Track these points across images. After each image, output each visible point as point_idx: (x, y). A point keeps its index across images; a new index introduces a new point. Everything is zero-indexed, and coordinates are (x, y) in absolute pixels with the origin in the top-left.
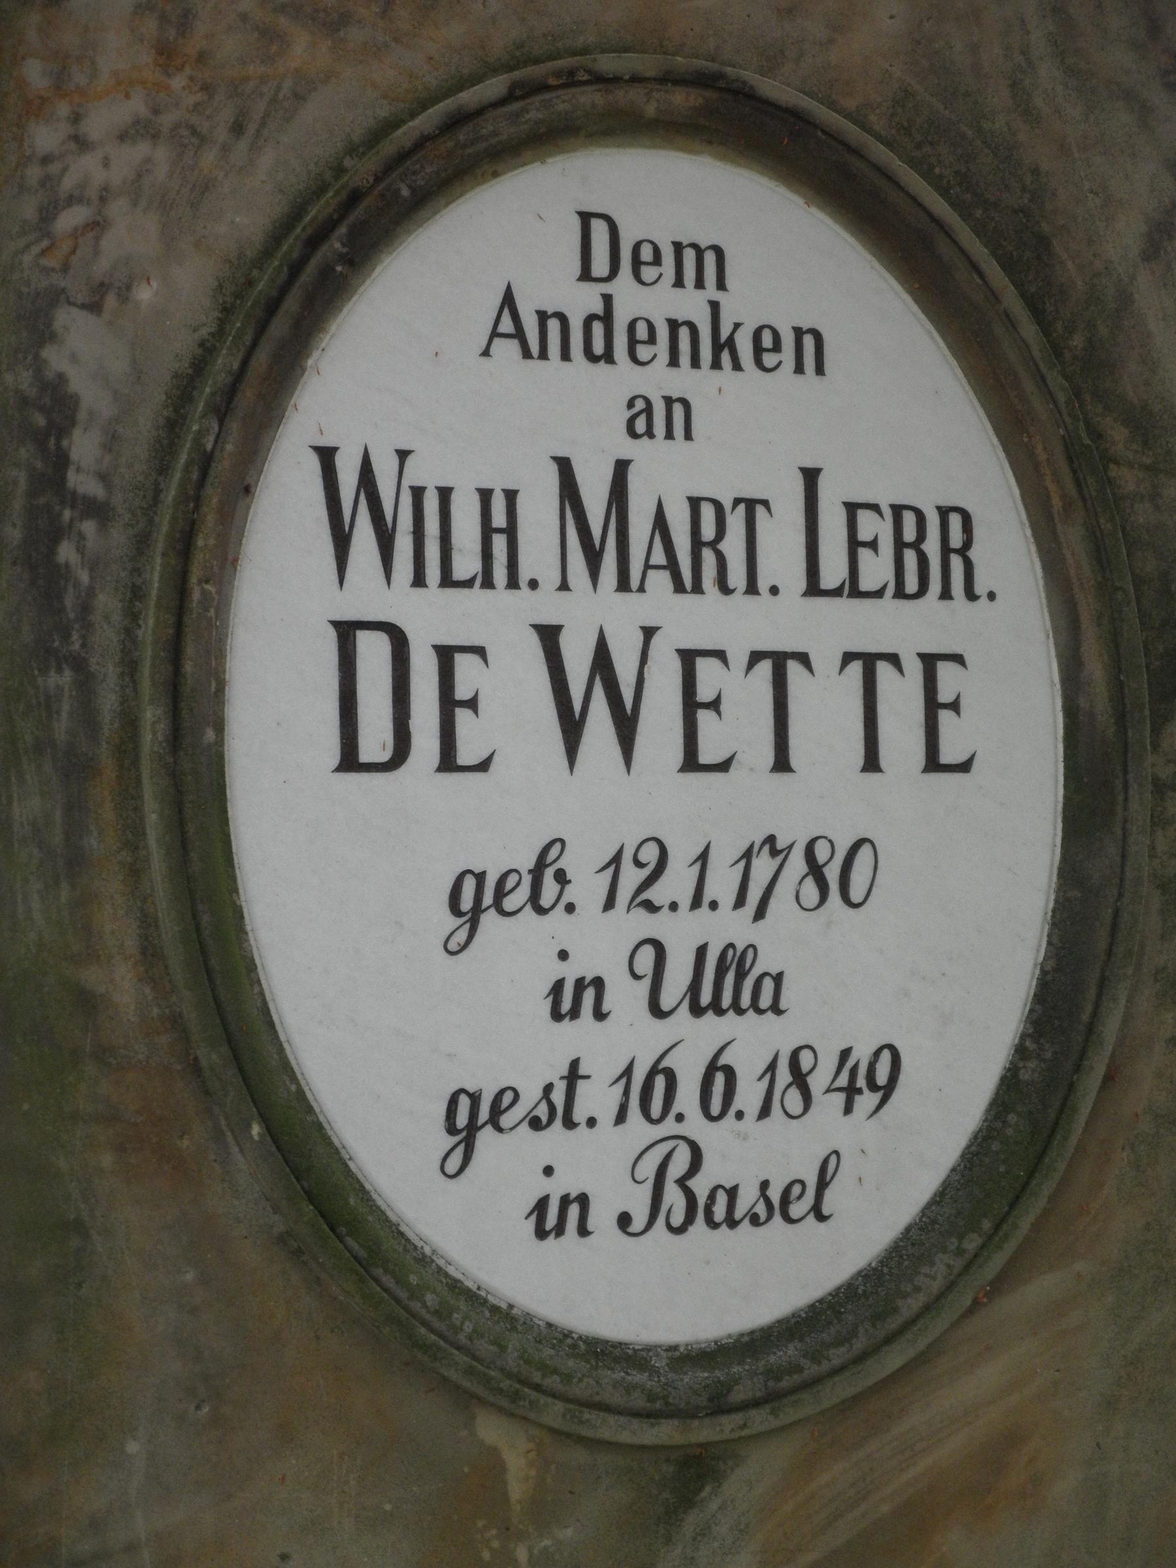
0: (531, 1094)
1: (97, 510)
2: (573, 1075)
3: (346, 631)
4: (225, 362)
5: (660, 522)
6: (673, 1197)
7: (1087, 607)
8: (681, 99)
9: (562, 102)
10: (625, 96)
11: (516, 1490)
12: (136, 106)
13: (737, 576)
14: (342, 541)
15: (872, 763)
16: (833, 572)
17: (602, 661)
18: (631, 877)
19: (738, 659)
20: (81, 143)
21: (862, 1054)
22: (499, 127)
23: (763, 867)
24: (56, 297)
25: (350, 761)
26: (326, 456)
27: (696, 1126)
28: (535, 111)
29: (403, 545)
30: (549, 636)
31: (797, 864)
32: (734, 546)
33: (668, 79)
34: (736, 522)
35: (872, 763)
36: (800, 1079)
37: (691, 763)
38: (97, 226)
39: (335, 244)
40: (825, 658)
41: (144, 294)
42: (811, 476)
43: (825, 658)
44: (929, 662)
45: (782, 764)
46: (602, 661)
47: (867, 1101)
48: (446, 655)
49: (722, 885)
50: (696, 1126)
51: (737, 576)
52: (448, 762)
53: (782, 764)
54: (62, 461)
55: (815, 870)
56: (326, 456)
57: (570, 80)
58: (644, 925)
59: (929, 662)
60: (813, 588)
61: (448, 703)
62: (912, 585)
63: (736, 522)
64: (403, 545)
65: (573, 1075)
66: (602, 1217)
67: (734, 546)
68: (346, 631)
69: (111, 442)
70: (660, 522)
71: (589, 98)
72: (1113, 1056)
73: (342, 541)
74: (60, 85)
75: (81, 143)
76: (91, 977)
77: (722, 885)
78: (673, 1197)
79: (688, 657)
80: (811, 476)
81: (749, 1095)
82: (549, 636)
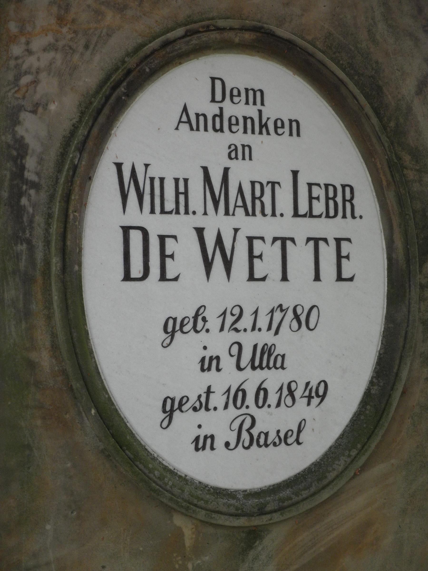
0: (193, 399)
1: (35, 186)
2: (209, 391)
3: (126, 230)
4: (82, 132)
5: (240, 190)
6: (245, 436)
7: (396, 221)
8: (248, 36)
9: (205, 37)
10: (227, 35)
11: (188, 543)
12: (50, 38)
13: (268, 210)
14: (124, 197)
15: (317, 278)
16: (303, 208)
17: (219, 241)
18: (230, 319)
19: (269, 240)
20: (30, 52)
21: (314, 384)
22: (181, 46)
23: (278, 316)
24: (21, 108)
25: (127, 277)
26: (119, 166)
27: (253, 410)
28: (195, 40)
29: (147, 198)
30: (200, 231)
31: (290, 315)
32: (267, 199)
33: (243, 29)
34: (268, 190)
35: (317, 278)
36: (291, 393)
37: (251, 278)
38: (35, 82)
39: (122, 89)
40: (300, 240)
41: (53, 107)
42: (295, 173)
43: (300, 240)
44: (338, 241)
45: (285, 278)
46: (219, 241)
47: (315, 401)
48: (162, 239)
49: (263, 322)
50: (253, 410)
51: (268, 210)
52: (163, 278)
53: (285, 278)
54: (23, 168)
55: (297, 317)
56: (119, 166)
57: (207, 29)
58: (234, 337)
59: (338, 241)
60: (296, 214)
61: (163, 256)
62: (332, 213)
63: (268, 190)
64: (147, 198)
65: (209, 391)
66: (219, 443)
67: (267, 199)
68: (126, 230)
69: (41, 161)
70: (240, 190)
71: (214, 36)
72: (405, 385)
73: (124, 197)
74: (22, 31)
75: (30, 52)
76: (33, 356)
77: (263, 322)
78: (245, 436)
79: (251, 239)
80: (295, 173)
81: (273, 399)
82: (200, 231)
